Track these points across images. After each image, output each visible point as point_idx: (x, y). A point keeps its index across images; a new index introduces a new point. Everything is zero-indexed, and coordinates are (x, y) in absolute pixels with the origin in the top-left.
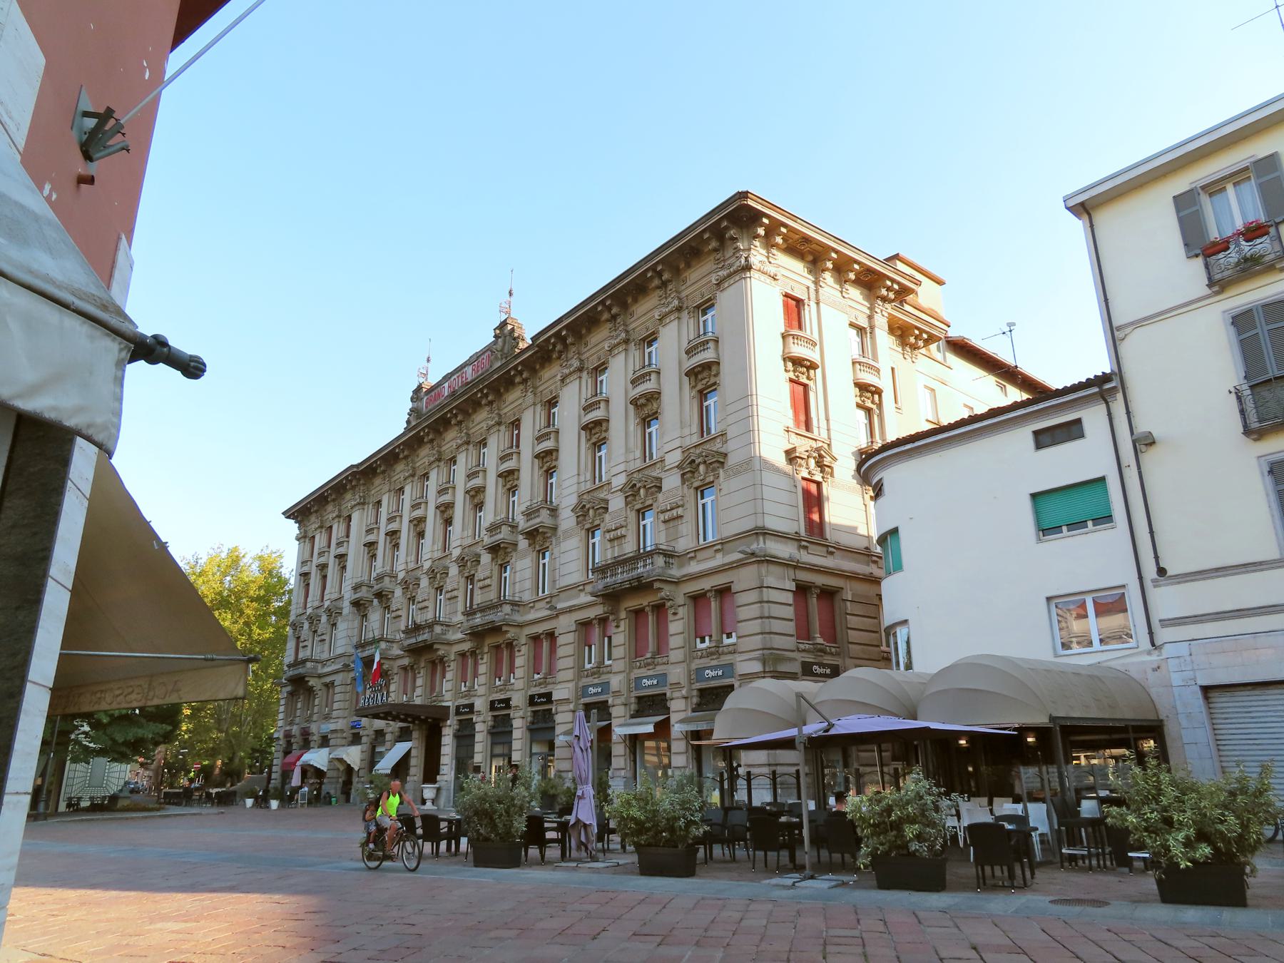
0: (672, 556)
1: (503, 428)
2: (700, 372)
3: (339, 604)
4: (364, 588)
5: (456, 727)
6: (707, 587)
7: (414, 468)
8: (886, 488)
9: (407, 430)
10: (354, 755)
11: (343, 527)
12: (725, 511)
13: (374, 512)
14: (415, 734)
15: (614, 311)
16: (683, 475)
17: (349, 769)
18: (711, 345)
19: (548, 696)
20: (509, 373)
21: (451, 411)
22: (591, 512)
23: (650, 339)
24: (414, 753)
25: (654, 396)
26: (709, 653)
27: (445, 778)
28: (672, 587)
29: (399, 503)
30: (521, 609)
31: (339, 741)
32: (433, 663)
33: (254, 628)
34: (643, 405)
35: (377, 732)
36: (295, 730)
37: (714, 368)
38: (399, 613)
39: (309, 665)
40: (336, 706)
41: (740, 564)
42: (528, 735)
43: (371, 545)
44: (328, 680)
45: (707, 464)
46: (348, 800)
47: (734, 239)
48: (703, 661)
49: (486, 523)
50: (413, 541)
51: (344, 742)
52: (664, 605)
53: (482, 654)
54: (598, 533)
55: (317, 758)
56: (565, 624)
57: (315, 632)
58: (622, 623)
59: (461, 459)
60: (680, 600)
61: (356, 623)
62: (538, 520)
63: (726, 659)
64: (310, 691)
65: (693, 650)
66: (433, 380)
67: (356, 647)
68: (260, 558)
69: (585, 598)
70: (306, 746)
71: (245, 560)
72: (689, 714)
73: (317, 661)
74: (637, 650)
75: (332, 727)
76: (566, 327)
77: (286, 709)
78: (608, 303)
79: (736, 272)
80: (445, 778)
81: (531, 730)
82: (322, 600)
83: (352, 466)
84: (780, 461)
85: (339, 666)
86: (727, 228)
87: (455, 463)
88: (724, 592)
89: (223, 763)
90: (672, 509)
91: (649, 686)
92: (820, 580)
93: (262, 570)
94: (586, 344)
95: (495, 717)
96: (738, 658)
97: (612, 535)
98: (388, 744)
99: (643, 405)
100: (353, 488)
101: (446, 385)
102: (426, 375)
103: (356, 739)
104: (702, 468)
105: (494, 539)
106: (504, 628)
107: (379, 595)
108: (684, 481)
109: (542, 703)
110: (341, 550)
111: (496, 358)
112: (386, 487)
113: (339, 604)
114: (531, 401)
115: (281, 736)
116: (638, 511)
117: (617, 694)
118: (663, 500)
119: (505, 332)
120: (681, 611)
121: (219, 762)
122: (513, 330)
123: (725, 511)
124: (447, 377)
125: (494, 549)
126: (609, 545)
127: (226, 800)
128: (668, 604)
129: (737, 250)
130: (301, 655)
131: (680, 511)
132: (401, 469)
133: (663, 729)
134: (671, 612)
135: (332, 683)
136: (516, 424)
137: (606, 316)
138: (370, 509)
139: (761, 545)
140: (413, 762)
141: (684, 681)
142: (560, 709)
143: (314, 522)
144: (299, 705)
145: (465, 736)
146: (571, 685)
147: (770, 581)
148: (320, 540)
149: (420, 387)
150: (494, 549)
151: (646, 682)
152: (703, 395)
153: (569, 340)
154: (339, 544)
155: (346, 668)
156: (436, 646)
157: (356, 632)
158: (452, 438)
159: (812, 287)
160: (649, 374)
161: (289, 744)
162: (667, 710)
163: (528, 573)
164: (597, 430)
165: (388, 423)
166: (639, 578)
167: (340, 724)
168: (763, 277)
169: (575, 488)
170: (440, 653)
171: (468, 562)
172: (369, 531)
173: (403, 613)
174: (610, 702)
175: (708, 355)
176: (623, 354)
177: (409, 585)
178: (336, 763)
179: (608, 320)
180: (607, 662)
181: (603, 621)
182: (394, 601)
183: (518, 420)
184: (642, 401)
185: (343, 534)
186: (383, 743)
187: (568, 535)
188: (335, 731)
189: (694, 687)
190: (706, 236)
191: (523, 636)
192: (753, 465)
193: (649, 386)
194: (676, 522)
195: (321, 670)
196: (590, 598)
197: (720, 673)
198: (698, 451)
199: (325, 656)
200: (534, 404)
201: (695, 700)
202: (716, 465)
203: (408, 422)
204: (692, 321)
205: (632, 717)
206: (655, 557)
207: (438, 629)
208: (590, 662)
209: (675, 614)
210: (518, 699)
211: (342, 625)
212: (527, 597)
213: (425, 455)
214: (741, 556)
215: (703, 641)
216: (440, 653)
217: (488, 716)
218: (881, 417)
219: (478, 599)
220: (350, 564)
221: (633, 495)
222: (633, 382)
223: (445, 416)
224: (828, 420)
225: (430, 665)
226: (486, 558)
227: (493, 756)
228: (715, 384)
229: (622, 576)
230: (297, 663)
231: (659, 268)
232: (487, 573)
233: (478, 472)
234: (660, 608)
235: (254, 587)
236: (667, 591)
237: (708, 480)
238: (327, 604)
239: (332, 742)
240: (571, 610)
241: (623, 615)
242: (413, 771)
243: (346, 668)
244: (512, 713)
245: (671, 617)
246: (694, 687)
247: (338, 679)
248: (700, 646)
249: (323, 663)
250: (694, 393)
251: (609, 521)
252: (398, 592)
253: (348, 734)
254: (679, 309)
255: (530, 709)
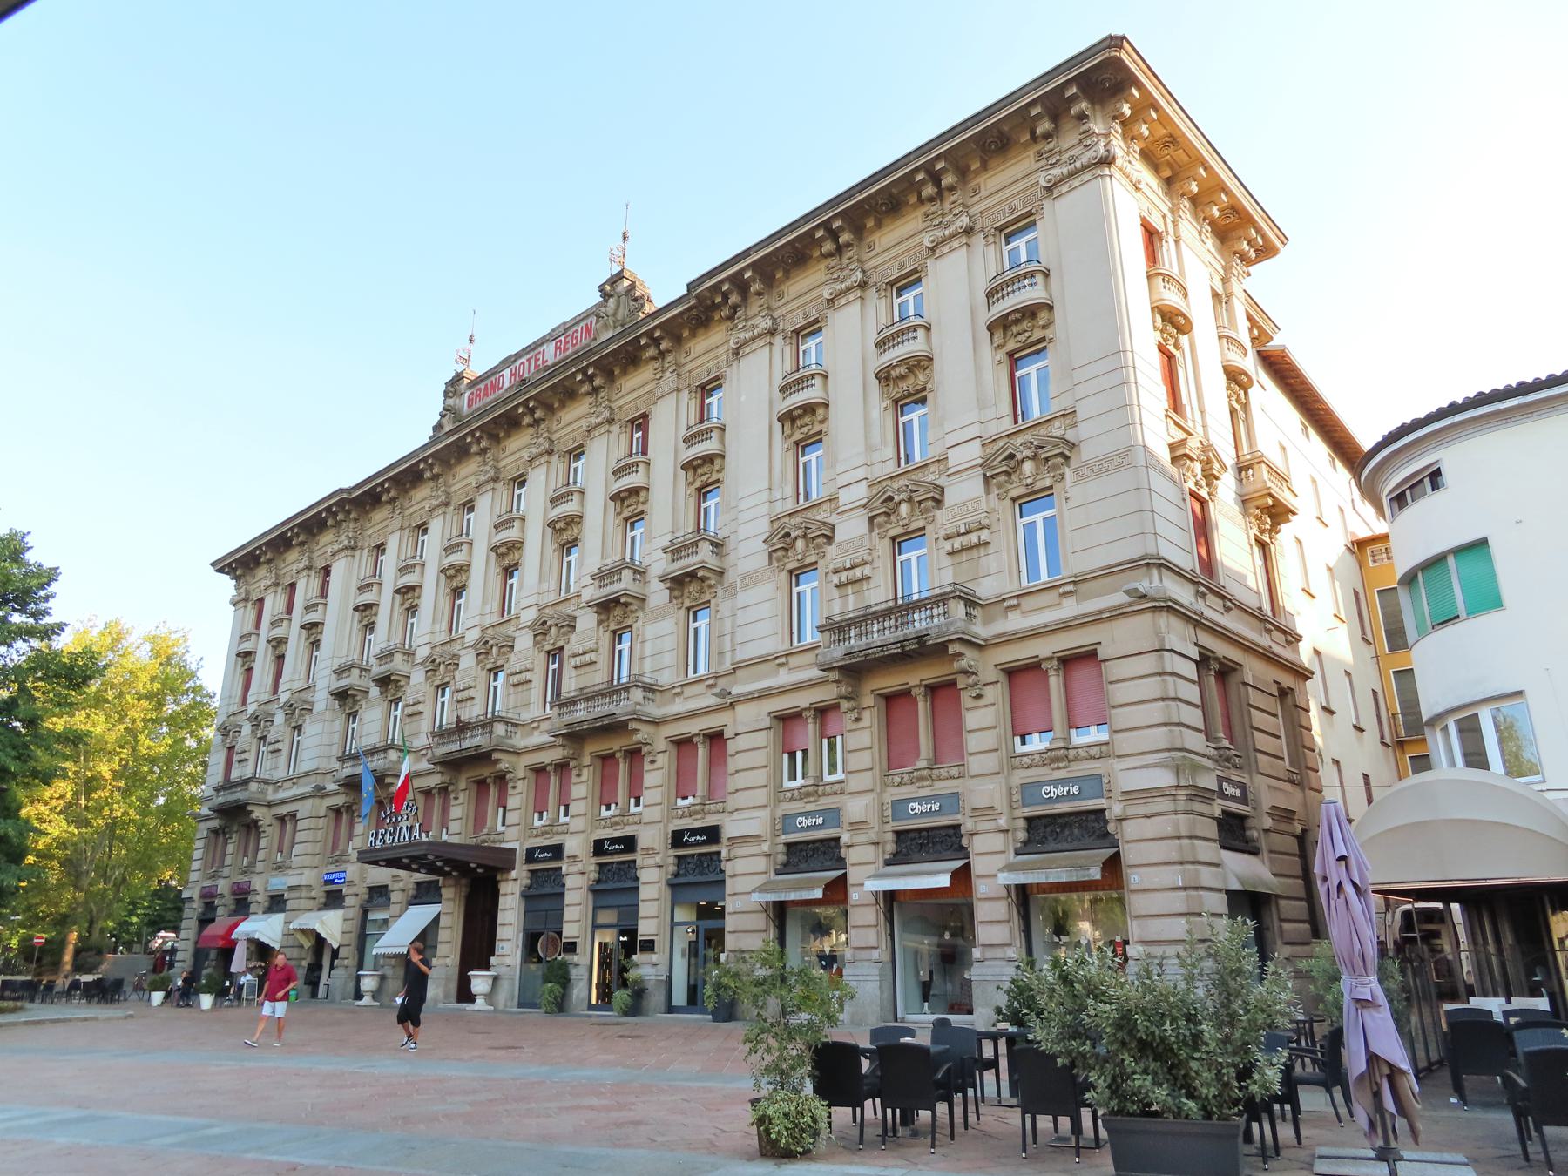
0: (654, 691)
1: (615, 428)
2: (700, 466)
3: (307, 696)
4: (355, 672)
5: (594, 876)
6: (694, 730)
7: (448, 494)
8: (1447, 475)
9: (434, 440)
10: (332, 925)
11: (315, 584)
12: (1089, 526)
13: (371, 561)
14: (447, 893)
15: (597, 382)
16: (871, 519)
17: (320, 942)
18: (715, 434)
19: (713, 834)
20: (619, 349)
21: (472, 433)
22: (553, 630)
23: (577, 453)
24: (443, 921)
25: (574, 520)
26: (803, 794)
27: (507, 961)
28: (513, 758)
29: (418, 548)
30: (658, 696)
31: (304, 904)
32: (482, 784)
33: (141, 737)
34: (562, 530)
35: (371, 889)
36: (223, 886)
37: (642, 494)
38: (419, 708)
39: (253, 786)
40: (297, 850)
41: (1118, 614)
42: (669, 892)
43: (366, 610)
44: (284, 810)
45: (1031, 463)
46: (314, 995)
47: (1082, 117)
48: (903, 789)
49: (375, 650)
50: (445, 601)
51: (311, 904)
52: (639, 750)
53: (580, 767)
54: (501, 675)
55: (265, 927)
56: (753, 716)
57: (263, 738)
58: (866, 715)
59: (435, 526)
60: (661, 744)
61: (338, 725)
62: (694, 559)
63: (827, 802)
64: (253, 827)
65: (779, 789)
66: (478, 368)
67: (342, 759)
68: (153, 639)
69: (539, 738)
70: (242, 907)
71: (131, 639)
72: (1012, 857)
73: (266, 783)
74: (895, 752)
75: (293, 881)
76: (753, 266)
77: (206, 854)
78: (590, 372)
79: (1085, 168)
80: (507, 961)
81: (595, 892)
82: (244, 702)
83: (341, 491)
84: (1165, 456)
85: (308, 789)
86: (1074, 99)
87: (425, 532)
88: (716, 738)
89: (80, 938)
90: (852, 568)
91: (922, 813)
92: (1222, 649)
93: (155, 654)
94: (781, 296)
95: (601, 865)
96: (1118, 765)
97: (843, 577)
98: (394, 909)
99: (562, 530)
100: (338, 524)
101: (507, 372)
102: (467, 361)
103: (334, 899)
104: (800, 544)
105: (383, 668)
106: (632, 725)
107: (384, 682)
108: (427, 679)
109: (545, 860)
110: (313, 617)
111: (606, 326)
112: (397, 523)
113: (307, 696)
114: (673, 386)
115: (196, 896)
116: (614, 632)
117: (857, 826)
118: (833, 555)
119: (618, 289)
120: (991, 694)
121: (73, 937)
122: (633, 286)
123: (1089, 526)
124: (507, 362)
125: (606, 607)
126: (836, 593)
127: (105, 992)
128: (645, 750)
129: (1088, 133)
130: (236, 774)
131: (867, 570)
132: (422, 496)
133: (837, 890)
134: (647, 759)
135: (293, 815)
136: (641, 422)
137: (586, 388)
138: (364, 559)
139: (1156, 583)
140: (443, 935)
141: (1000, 803)
142: (739, 851)
143: (263, 576)
144: (230, 848)
145: (545, 895)
146: (764, 814)
147: (1173, 641)
148: (274, 604)
149: (459, 377)
150: (606, 607)
151: (803, 821)
152: (703, 493)
153: (756, 287)
154: (309, 608)
155: (320, 792)
156: (495, 756)
157: (337, 738)
158: (518, 446)
159: (1170, 218)
160: (571, 493)
161: (210, 907)
162: (841, 862)
163: (670, 643)
164: (632, 500)
165: (409, 428)
166: (920, 638)
167: (307, 877)
168: (1125, 181)
169: (765, 509)
170: (502, 766)
171: (552, 629)
172: (364, 588)
173: (427, 708)
174: (564, 870)
175: (913, 347)
176: (857, 305)
177: (440, 667)
178: (299, 936)
179: (529, 425)
180: (563, 819)
181: (562, 767)
182: (408, 690)
183: (645, 416)
184: (561, 525)
185: (369, 572)
186: (387, 904)
187: (749, 580)
188: (298, 888)
189: (1018, 813)
190: (919, 177)
191: (987, 666)
192: (1127, 456)
193: (570, 508)
194: (974, 553)
195: (271, 796)
196: (815, 673)
197: (820, 821)
198: (793, 522)
199: (280, 774)
200: (678, 390)
201: (411, 892)
202: (821, 540)
203: (438, 427)
204: (787, 349)
205: (888, 863)
206: (633, 690)
207: (500, 729)
208: (793, 777)
209: (653, 762)
210: (652, 837)
211: (311, 728)
212: (666, 678)
213: (468, 473)
214: (1126, 599)
215: (608, 808)
216: (502, 766)
217: (591, 864)
218: (1247, 421)
219: (570, 686)
220: (327, 637)
221: (887, 514)
222: (783, 390)
223: (492, 422)
224: (1202, 412)
225: (474, 787)
226: (587, 621)
227: (596, 927)
228: (717, 481)
229: (879, 636)
230: (227, 785)
231: (657, 334)
232: (591, 644)
233: (413, 566)
234: (634, 754)
235: (144, 677)
236: (970, 658)
237: (808, 560)
238: (251, 708)
239: (289, 905)
240: (760, 696)
241: (868, 700)
242: (442, 949)
243: (320, 792)
244: (638, 858)
245: (647, 766)
246: (1018, 813)
247: (303, 809)
248: (605, 813)
249: (277, 784)
250: (1001, 355)
251: (514, 662)
252: (418, 676)
253: (319, 893)
254: (863, 285)
255: (672, 852)
